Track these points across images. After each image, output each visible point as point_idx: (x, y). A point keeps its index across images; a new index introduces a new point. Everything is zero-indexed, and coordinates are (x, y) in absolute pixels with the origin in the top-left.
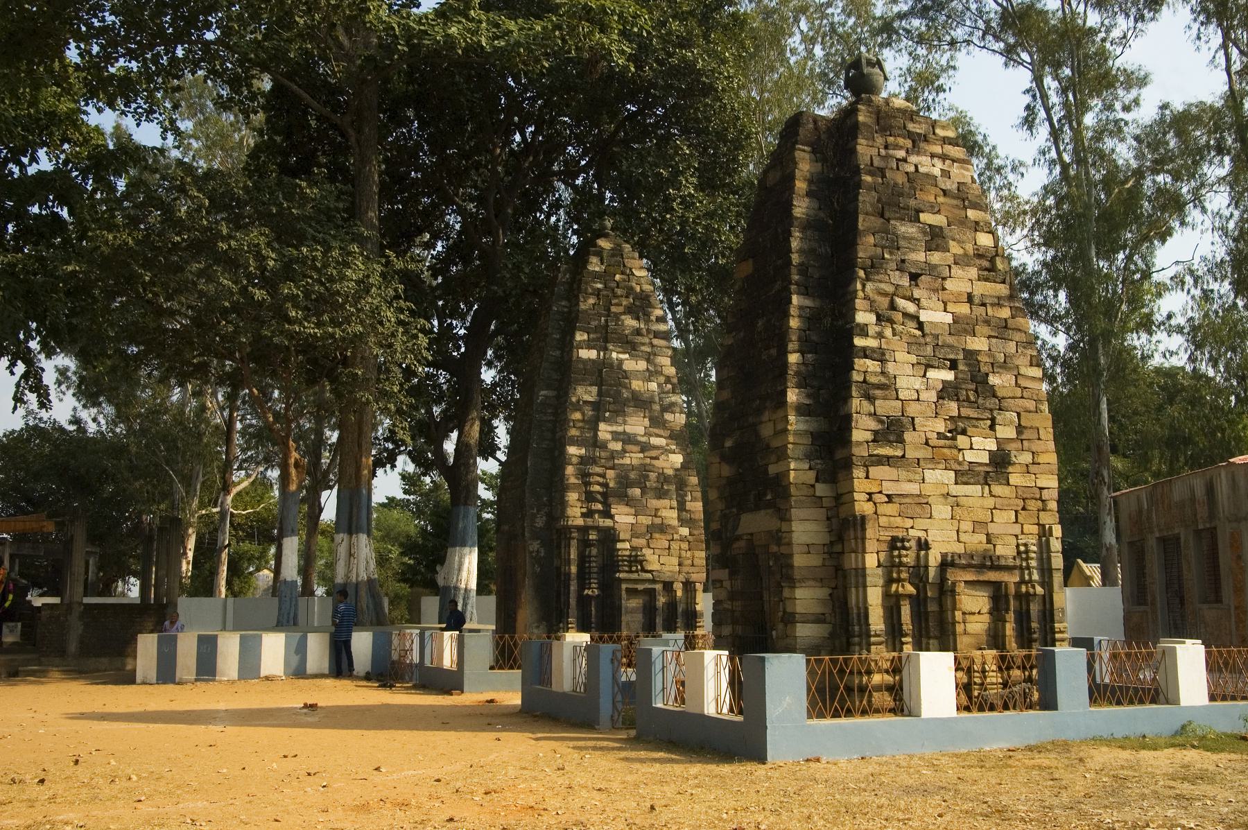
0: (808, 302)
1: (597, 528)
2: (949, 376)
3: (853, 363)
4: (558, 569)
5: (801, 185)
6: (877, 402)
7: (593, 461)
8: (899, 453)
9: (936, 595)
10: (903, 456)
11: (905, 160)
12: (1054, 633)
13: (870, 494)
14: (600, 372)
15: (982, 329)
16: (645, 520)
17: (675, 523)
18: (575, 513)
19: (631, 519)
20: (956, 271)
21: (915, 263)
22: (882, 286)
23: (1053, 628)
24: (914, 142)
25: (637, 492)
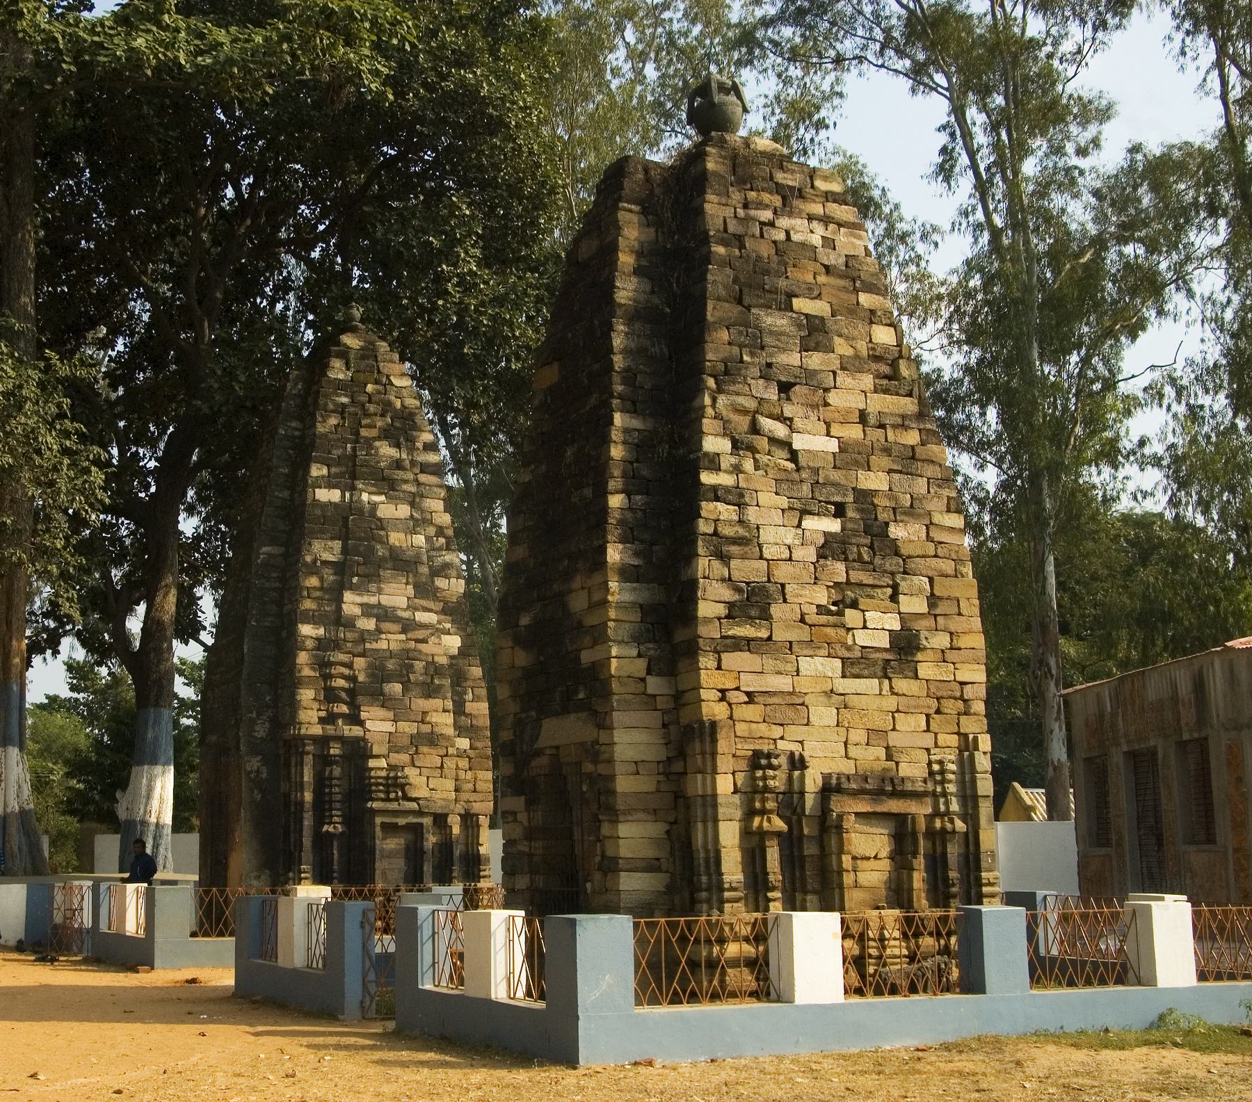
0: (636, 423)
1: (341, 739)
2: (834, 526)
3: (699, 508)
4: (287, 796)
5: (626, 259)
6: (733, 563)
8: (764, 634)
9: (815, 833)
10: (770, 638)
11: (772, 224)
12: (981, 885)
13: (723, 691)
16: (408, 728)
17: (450, 731)
18: (310, 718)
19: (388, 727)
20: (842, 378)
21: (787, 367)
23: (978, 879)
24: (784, 198)
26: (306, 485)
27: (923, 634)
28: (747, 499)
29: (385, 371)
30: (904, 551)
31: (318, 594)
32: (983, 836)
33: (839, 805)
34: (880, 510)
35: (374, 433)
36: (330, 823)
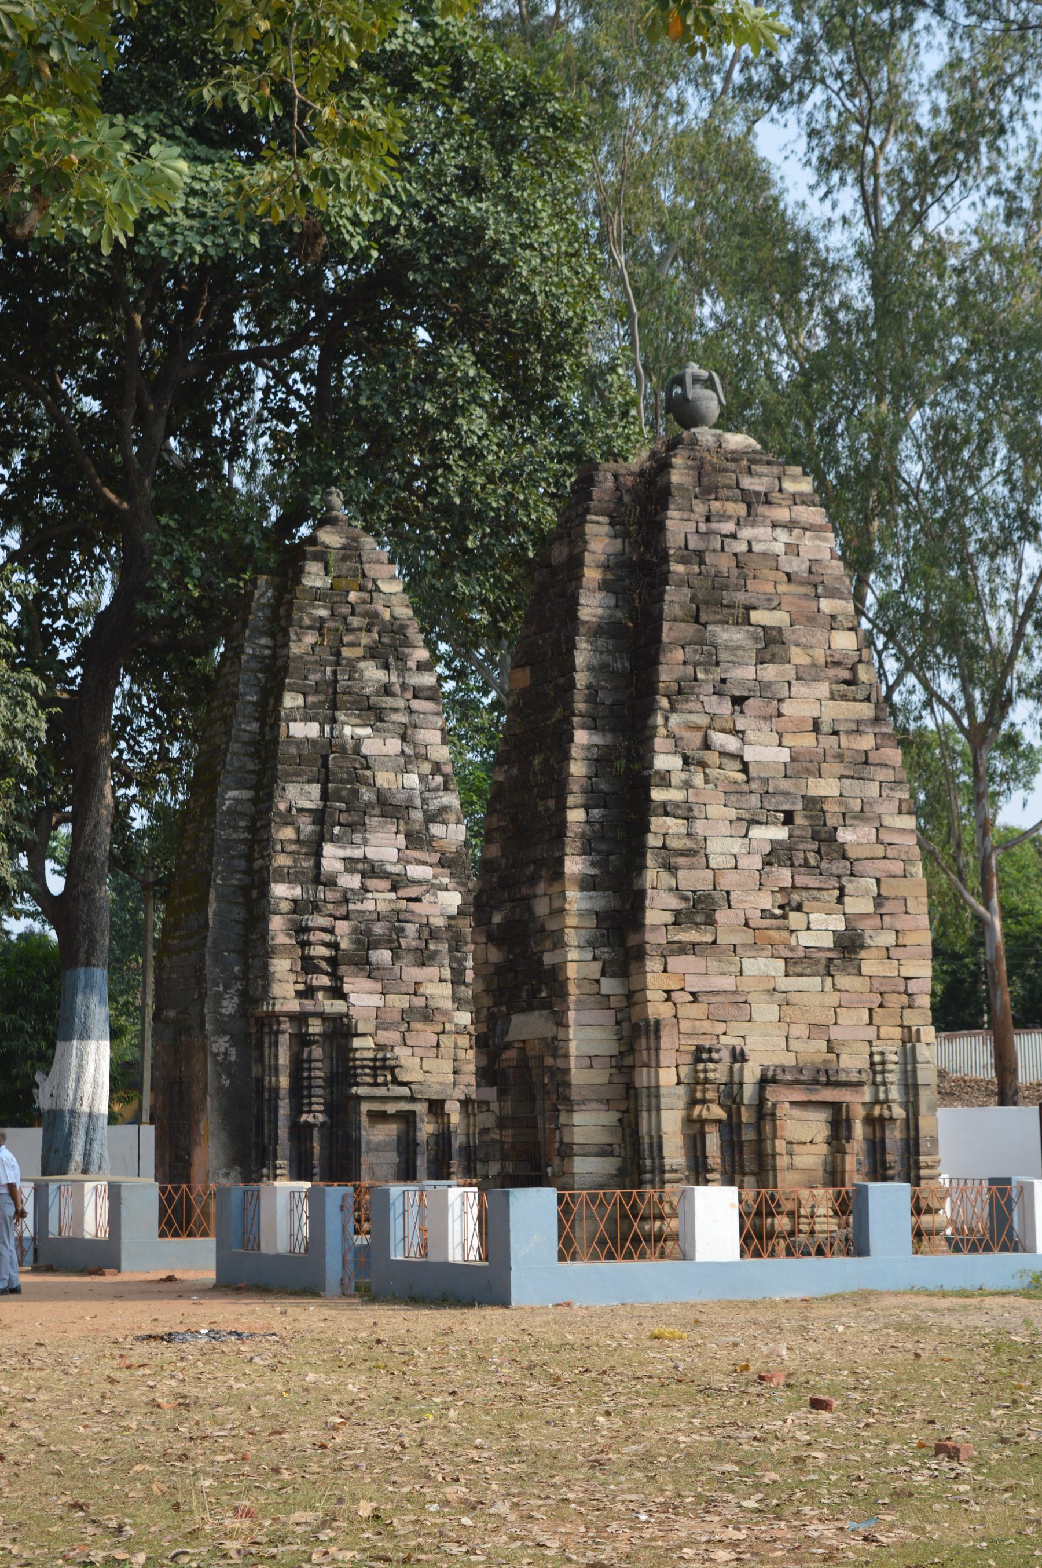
0: (597, 739)
1: (322, 1016)
2: (781, 833)
3: (648, 823)
4: (260, 1081)
5: (592, 575)
6: (681, 874)
7: (315, 907)
8: (709, 939)
9: (753, 1120)
10: (714, 942)
11: (734, 536)
12: (919, 1168)
13: (668, 992)
14: (325, 758)
15: (832, 768)
16: (399, 1002)
17: (448, 1004)
18: (285, 990)
19: (376, 1001)
20: (798, 688)
21: (740, 682)
22: (693, 718)
23: (917, 1162)
24: (749, 506)
25: (383, 956)
26: (278, 718)
27: (868, 933)
28: (696, 813)
29: (371, 574)
30: (852, 854)
31: (293, 847)
32: (922, 1122)
33: (772, 1094)
34: (828, 815)
35: (358, 652)
36: (309, 1112)
